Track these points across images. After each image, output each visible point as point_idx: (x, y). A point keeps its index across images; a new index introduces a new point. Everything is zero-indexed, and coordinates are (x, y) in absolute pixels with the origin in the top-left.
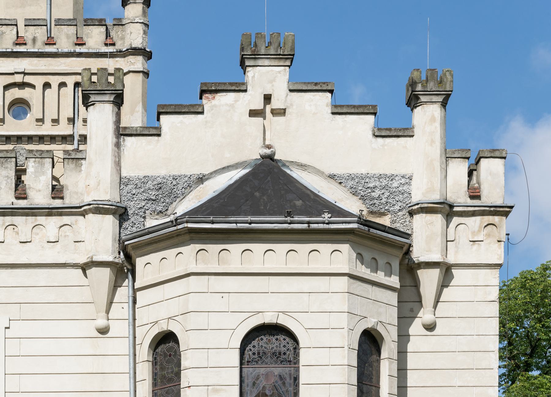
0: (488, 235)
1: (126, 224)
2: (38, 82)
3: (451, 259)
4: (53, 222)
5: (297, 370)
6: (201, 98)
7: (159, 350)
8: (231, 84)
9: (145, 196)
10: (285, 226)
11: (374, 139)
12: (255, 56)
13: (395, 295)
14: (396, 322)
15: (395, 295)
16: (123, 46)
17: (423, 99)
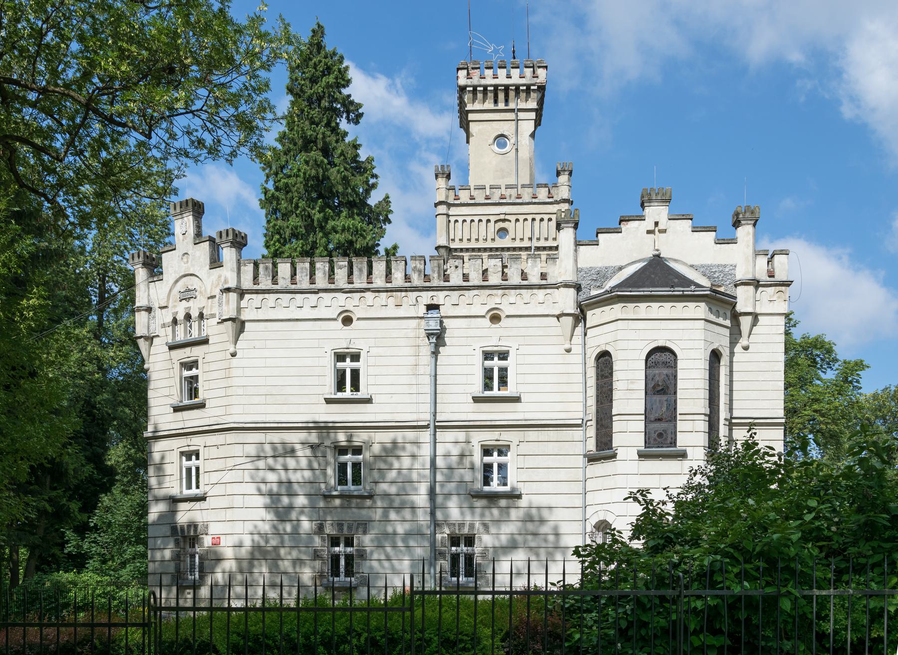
0: (779, 297)
1: (580, 293)
2: (513, 218)
3: (758, 311)
4: (541, 293)
5: (676, 371)
6: (620, 224)
7: (600, 360)
8: (637, 216)
9: (591, 278)
10: (670, 293)
11: (715, 245)
12: (650, 201)
13: (728, 330)
14: (728, 345)
15: (728, 330)
16: (557, 198)
17: (743, 222)
